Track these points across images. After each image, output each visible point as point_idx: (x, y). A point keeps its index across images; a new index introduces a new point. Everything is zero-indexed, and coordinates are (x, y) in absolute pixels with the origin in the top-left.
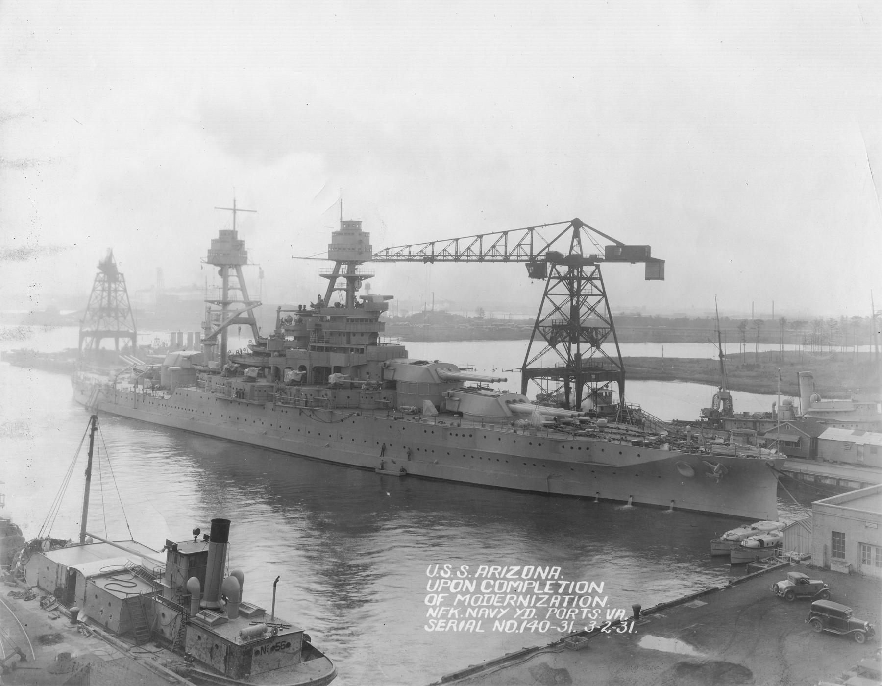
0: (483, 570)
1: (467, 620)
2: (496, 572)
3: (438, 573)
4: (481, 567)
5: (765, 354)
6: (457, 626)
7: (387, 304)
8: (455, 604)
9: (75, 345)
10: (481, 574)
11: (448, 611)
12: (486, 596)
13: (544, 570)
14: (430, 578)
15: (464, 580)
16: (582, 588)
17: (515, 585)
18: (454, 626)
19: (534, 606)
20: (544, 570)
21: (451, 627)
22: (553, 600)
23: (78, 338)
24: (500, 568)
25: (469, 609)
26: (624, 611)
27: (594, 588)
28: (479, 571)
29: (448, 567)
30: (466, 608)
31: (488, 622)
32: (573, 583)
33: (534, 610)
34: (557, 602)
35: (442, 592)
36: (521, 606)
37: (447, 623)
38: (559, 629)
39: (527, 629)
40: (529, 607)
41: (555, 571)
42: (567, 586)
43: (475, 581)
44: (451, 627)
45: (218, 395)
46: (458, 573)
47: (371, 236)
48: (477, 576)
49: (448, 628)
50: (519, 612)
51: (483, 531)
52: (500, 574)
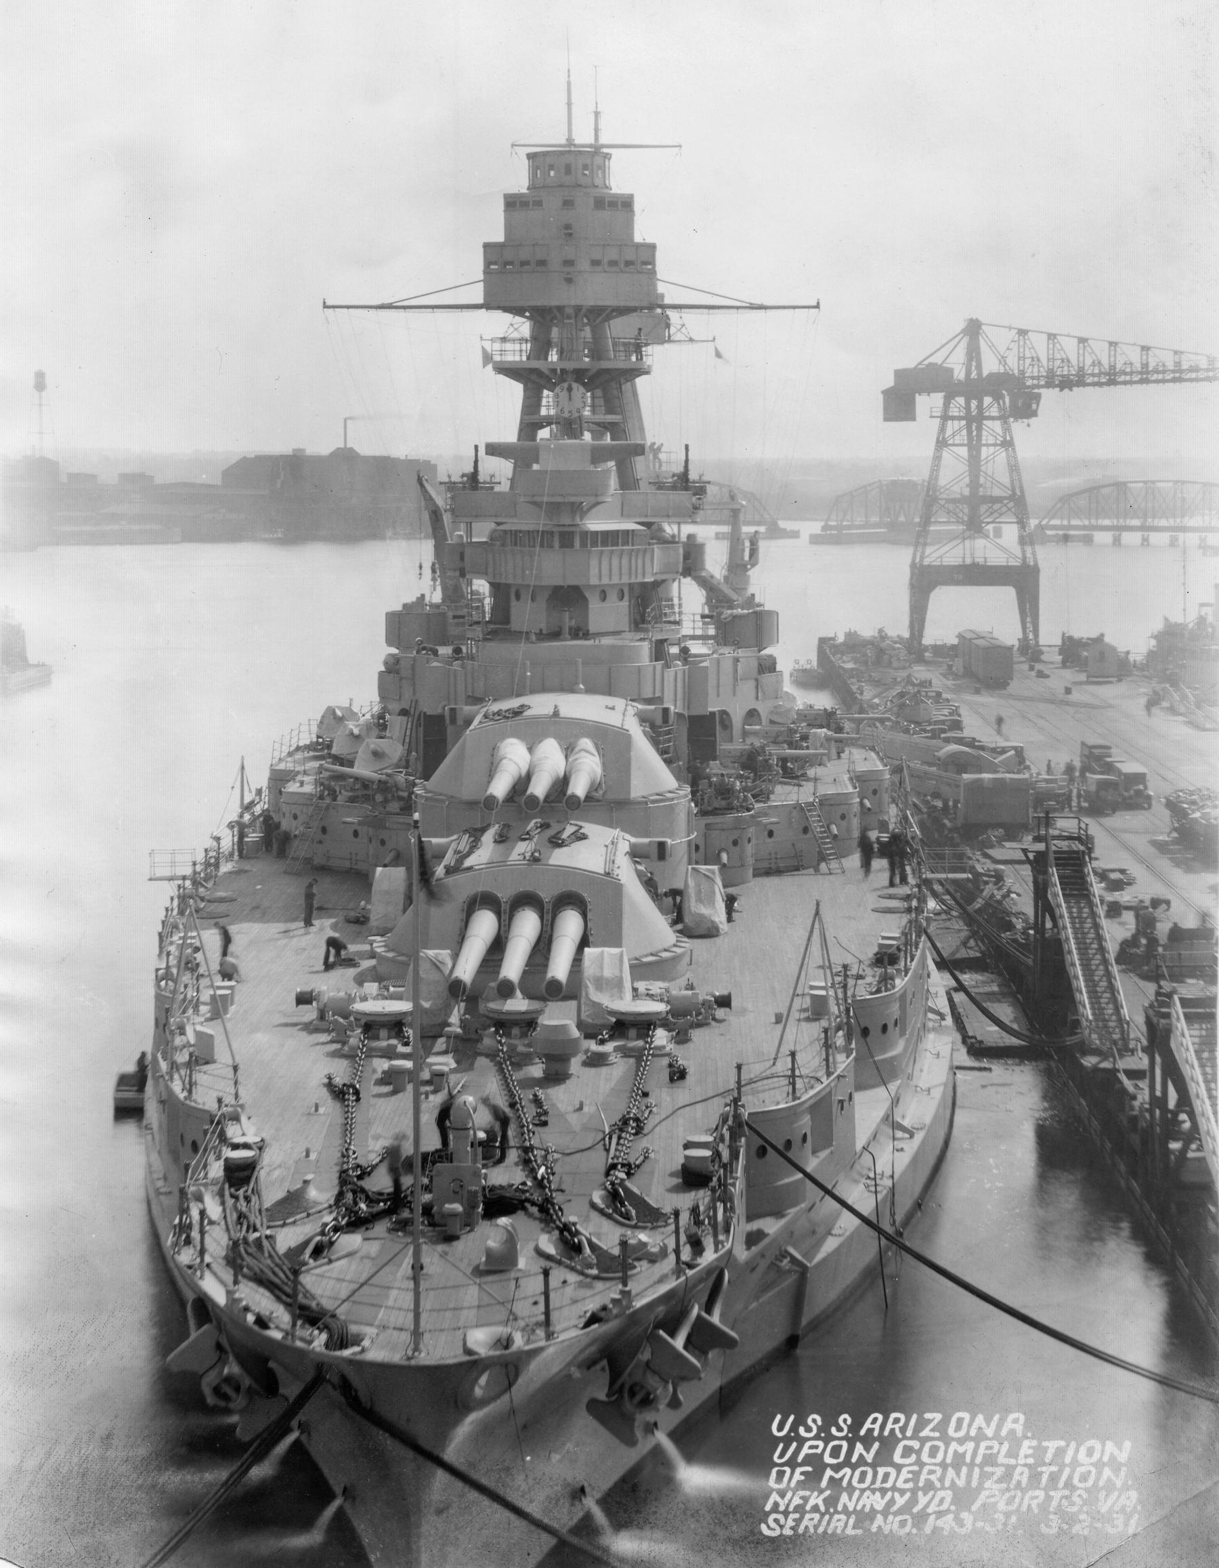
2: (897, 1427)
3: (794, 1428)
4: (873, 1416)
5: (1071, 971)
9: (819, 532)
10: (870, 1431)
13: (988, 1423)
16: (1090, 1452)
17: (961, 1450)
23: (780, 542)
27: (861, 1455)
28: (868, 1425)
29: (814, 1421)
32: (1073, 1445)
35: (802, 1464)
42: (1060, 1452)
45: (879, 893)
47: (900, 367)
48: (862, 1432)
51: (350, 1412)
52: (903, 1430)
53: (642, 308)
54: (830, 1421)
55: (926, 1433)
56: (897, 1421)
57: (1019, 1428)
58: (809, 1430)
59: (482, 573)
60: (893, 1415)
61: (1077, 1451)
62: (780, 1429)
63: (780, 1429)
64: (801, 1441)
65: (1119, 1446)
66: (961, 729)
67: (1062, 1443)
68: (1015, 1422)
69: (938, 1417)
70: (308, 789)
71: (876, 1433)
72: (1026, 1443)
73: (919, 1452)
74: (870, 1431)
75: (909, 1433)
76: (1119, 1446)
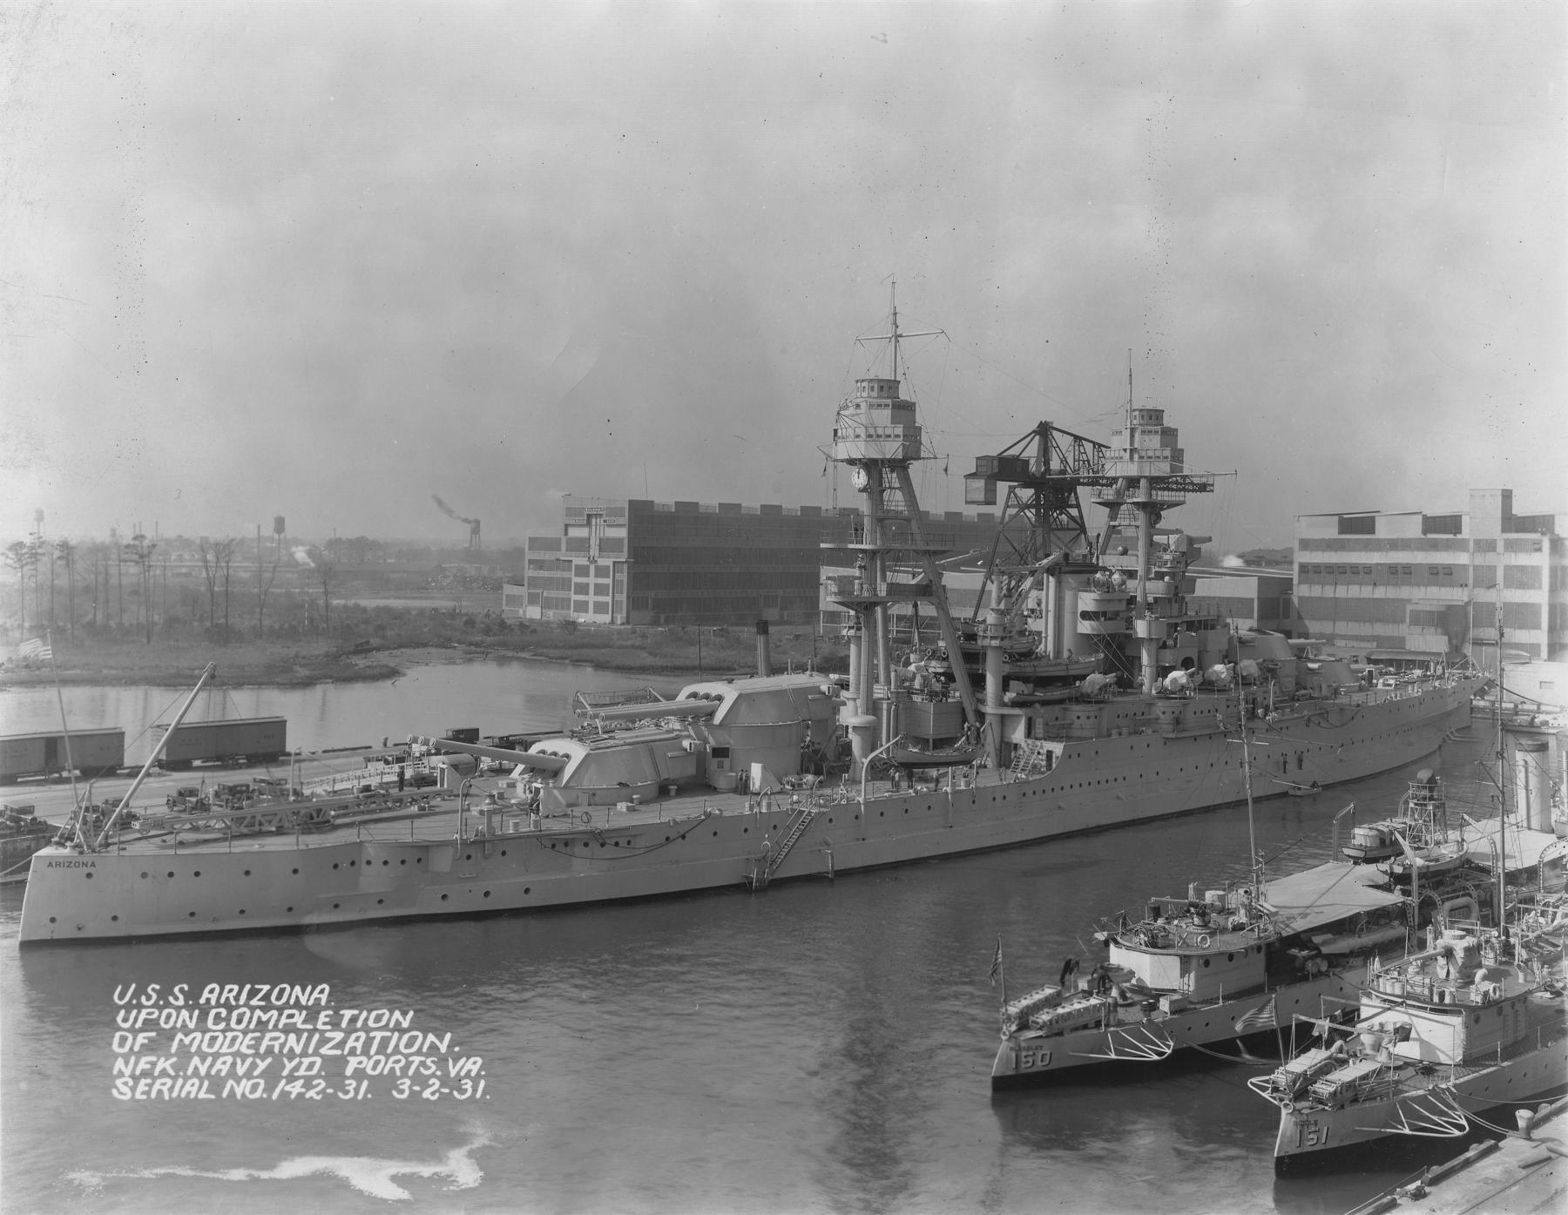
0: (212, 991)
1: (186, 1078)
3: (136, 995)
6: (171, 1089)
7: (1341, 532)
8: (173, 1050)
10: (208, 1000)
11: (154, 1064)
12: (378, 1035)
13: (303, 991)
14: (121, 1007)
15: (178, 1009)
17: (264, 1018)
18: (165, 1089)
19: (316, 1053)
20: (303, 991)
21: (160, 1092)
22: (351, 1043)
24: (236, 988)
25: (196, 1060)
26: (479, 1061)
30: (191, 1056)
31: (216, 1083)
32: (365, 1014)
33: (319, 1061)
34: (359, 1045)
35: (141, 1030)
36: (291, 1055)
37: (150, 1086)
38: (341, 1095)
39: (285, 1094)
40: (304, 1054)
41: (322, 991)
43: (196, 1012)
44: (160, 1092)
46: (143, 998)
49: (153, 1095)
50: (289, 1066)
52: (237, 998)
53: (1433, 753)
54: (164, 994)
55: (254, 1002)
56: (231, 991)
57: (324, 998)
58: (149, 998)
59: (1226, 554)
60: (228, 987)
61: (400, 1039)
62: (121, 997)
63: (121, 997)
64: (140, 1007)
65: (404, 1014)
66: (1372, 531)
67: (356, 1012)
68: (322, 992)
69: (266, 988)
70: (1357, 831)
71: (213, 1002)
72: (323, 1013)
73: (228, 1019)
74: (208, 1000)
75: (242, 1002)
76: (404, 1014)
